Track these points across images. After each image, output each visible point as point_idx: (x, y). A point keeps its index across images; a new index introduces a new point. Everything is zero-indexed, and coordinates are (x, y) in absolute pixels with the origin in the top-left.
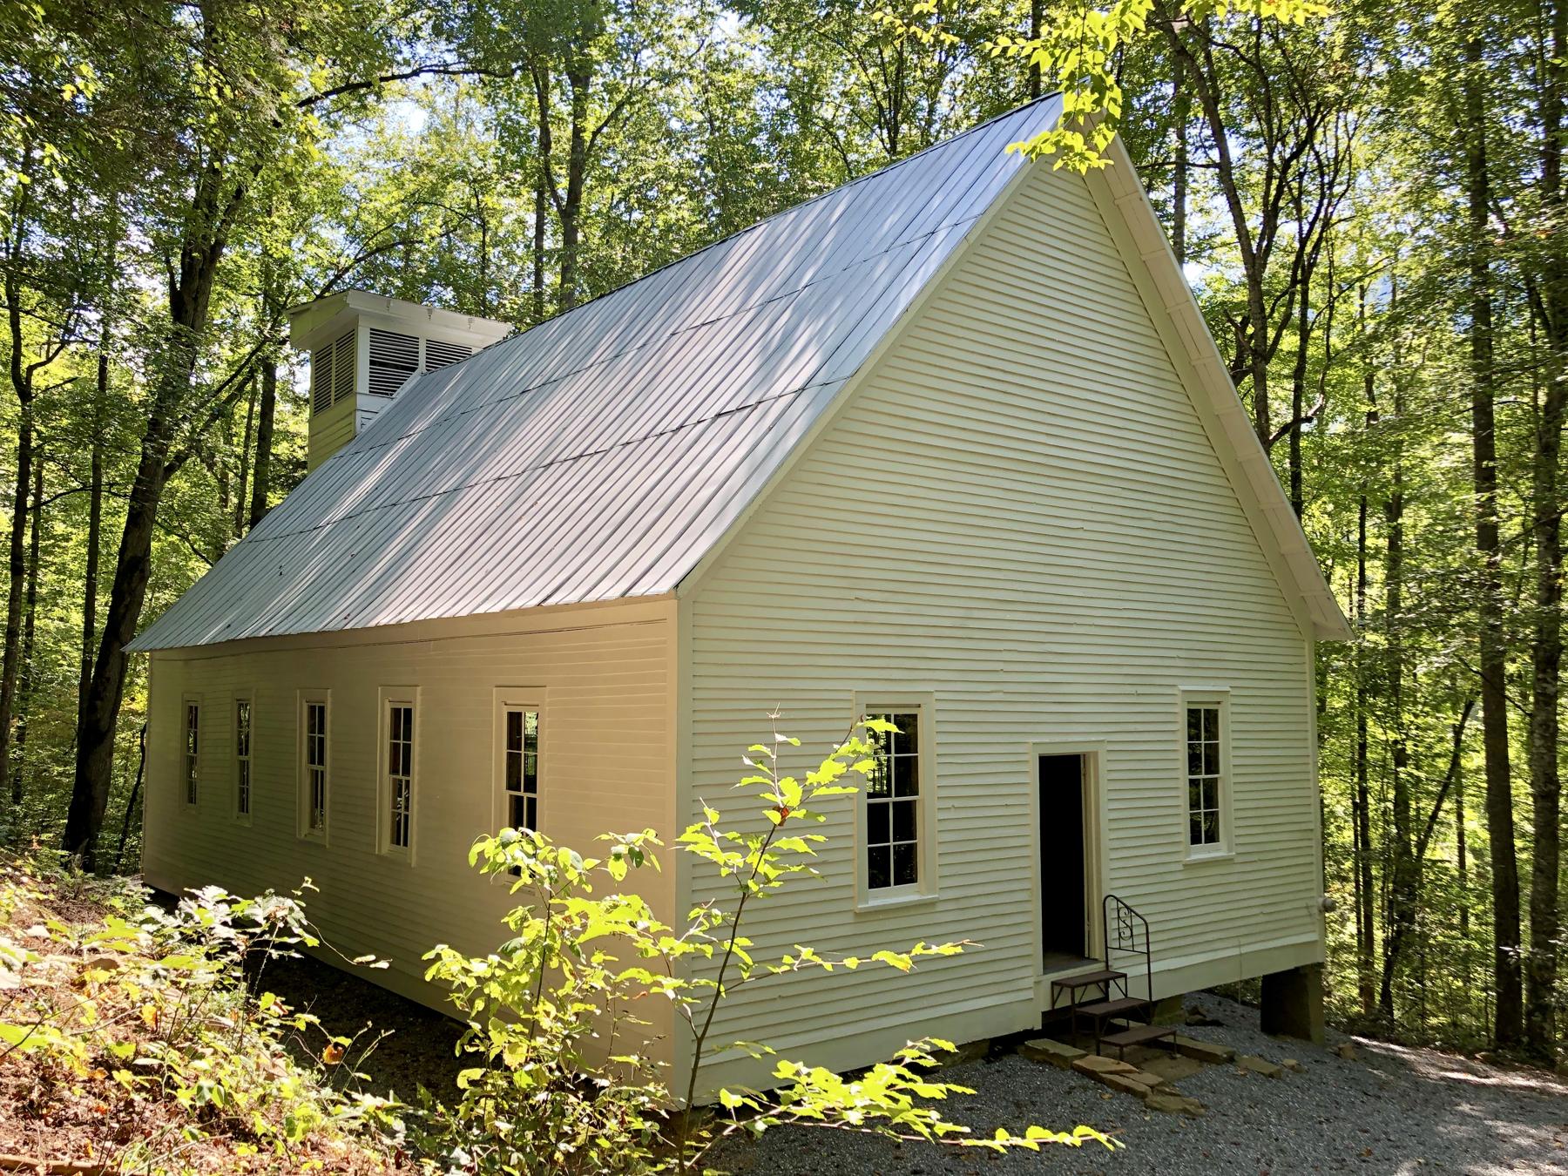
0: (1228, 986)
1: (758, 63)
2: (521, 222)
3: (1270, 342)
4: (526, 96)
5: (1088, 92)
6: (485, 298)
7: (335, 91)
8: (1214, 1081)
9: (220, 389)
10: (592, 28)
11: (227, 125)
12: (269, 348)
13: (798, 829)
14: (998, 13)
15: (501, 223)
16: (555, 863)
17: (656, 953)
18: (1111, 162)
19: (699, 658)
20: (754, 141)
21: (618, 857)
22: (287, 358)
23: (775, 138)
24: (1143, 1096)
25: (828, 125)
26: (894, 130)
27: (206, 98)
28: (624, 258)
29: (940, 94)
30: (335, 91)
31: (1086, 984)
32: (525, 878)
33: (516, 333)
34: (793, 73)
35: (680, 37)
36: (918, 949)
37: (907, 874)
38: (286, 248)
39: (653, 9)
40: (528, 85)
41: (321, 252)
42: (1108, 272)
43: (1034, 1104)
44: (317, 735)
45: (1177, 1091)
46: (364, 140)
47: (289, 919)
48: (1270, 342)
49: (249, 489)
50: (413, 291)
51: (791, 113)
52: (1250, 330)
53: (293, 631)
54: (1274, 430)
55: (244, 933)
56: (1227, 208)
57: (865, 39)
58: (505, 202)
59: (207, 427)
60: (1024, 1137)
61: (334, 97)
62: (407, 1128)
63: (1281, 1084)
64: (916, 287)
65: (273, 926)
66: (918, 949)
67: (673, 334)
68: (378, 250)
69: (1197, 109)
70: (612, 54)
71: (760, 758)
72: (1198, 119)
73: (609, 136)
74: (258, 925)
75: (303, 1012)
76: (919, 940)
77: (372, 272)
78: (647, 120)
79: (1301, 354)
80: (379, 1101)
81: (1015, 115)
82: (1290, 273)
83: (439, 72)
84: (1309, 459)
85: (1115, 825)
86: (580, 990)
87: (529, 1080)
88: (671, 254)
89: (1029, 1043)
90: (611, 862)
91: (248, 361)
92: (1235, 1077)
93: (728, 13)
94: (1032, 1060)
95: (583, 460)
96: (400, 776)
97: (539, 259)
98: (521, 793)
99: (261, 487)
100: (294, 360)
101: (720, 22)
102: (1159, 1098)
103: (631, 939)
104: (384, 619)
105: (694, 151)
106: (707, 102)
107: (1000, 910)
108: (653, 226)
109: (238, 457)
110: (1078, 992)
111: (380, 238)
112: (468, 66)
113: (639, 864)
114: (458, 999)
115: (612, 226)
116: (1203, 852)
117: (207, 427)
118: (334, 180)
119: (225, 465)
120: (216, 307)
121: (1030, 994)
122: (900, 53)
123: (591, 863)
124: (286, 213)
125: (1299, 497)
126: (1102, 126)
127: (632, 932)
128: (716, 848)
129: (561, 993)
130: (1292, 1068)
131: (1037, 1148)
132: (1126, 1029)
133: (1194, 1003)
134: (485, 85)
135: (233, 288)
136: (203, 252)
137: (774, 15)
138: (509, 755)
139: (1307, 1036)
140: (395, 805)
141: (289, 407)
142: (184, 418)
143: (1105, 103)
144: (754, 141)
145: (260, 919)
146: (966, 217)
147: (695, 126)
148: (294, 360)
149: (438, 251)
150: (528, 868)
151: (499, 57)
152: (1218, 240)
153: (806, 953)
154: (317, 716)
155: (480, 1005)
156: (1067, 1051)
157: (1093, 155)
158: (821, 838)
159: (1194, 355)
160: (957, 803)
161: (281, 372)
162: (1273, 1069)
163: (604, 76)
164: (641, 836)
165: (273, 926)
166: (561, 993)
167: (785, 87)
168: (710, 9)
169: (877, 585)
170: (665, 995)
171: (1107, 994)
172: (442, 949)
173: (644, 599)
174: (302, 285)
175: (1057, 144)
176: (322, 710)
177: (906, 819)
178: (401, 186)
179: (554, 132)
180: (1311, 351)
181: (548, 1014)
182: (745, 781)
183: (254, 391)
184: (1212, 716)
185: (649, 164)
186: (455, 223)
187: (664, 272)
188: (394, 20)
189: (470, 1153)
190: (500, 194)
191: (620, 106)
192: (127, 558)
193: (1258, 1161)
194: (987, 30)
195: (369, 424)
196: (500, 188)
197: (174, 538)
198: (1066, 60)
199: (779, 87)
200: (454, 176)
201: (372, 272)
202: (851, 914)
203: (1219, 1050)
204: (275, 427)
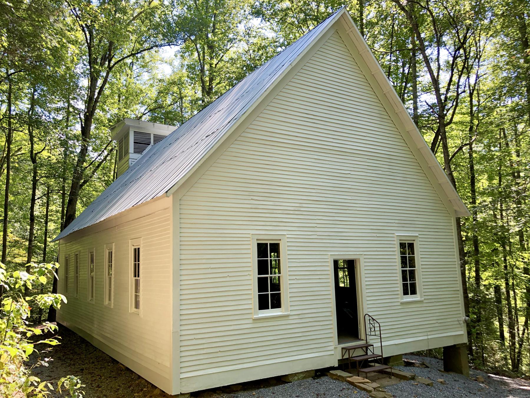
0: (418, 352)
8: (403, 387)
24: (370, 391)
31: (355, 349)
37: (277, 304)
63: (433, 388)
85: (368, 287)
92: (413, 385)
94: (332, 378)
110: (351, 351)
116: (410, 298)
121: (332, 352)
130: (441, 382)
139: (461, 373)
159: (396, 109)
160: (298, 277)
162: (430, 382)
184: (411, 246)
192: (68, 215)
195: (134, 163)
202: (251, 320)
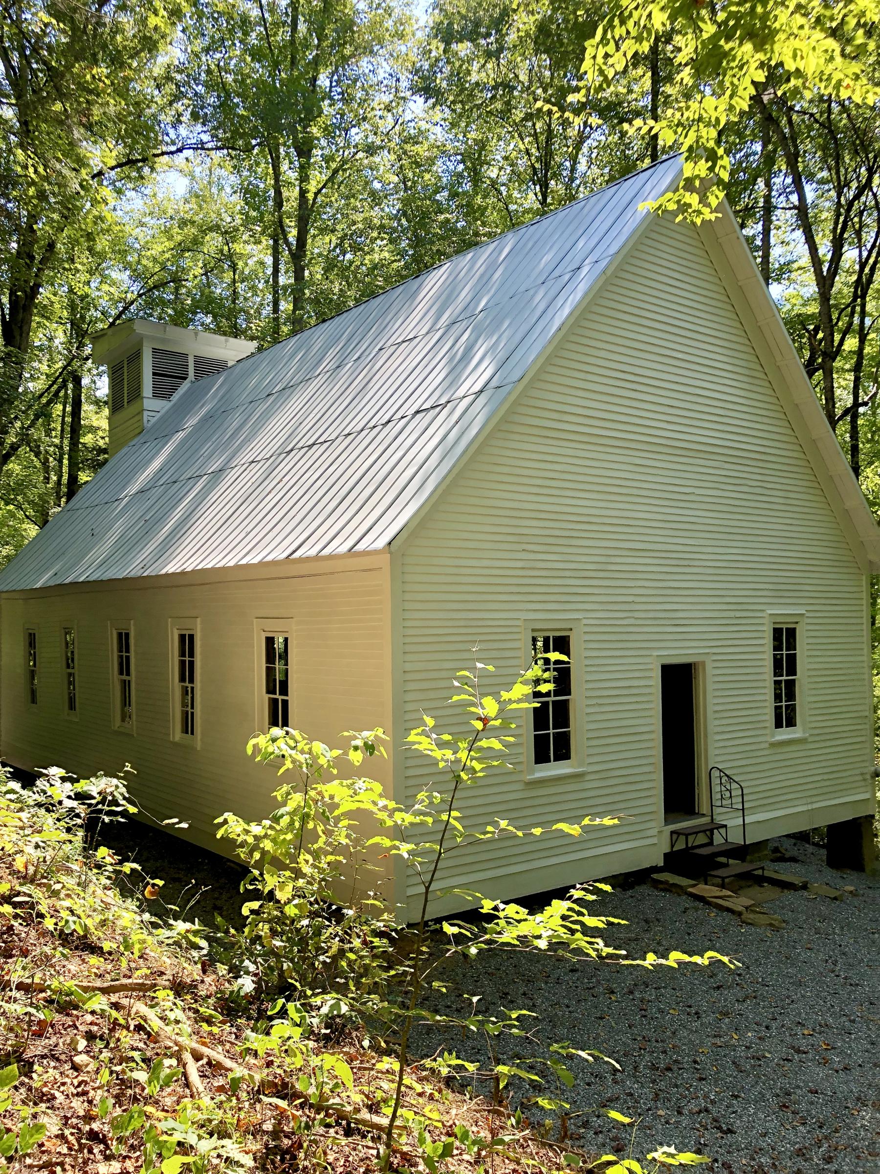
0: (801, 832)
1: (439, 136)
2: (262, 263)
3: (836, 344)
4: (263, 165)
5: (703, 161)
6: (236, 323)
7: (120, 165)
9: (41, 396)
10: (312, 111)
11: (42, 196)
12: (76, 364)
13: (495, 733)
14: (625, 91)
15: (246, 264)
16: (310, 752)
17: (392, 824)
18: (720, 215)
19: (407, 597)
20: (438, 197)
21: (356, 748)
22: (89, 370)
23: (454, 195)
24: (740, 914)
25: (494, 183)
26: (545, 186)
27: (26, 176)
28: (341, 290)
29: (580, 156)
30: (120, 165)
31: (697, 833)
32: (288, 764)
33: (260, 349)
34: (466, 143)
35: (381, 118)
36: (586, 821)
37: (563, 752)
38: (86, 287)
39: (359, 95)
40: (265, 157)
41: (112, 290)
42: (742, 393)
43: (658, 920)
44: (124, 654)
45: (764, 910)
46: (141, 202)
47: (115, 793)
48: (836, 344)
49: (65, 469)
50: (181, 319)
51: (466, 174)
52: (820, 335)
53: (105, 577)
54: (839, 412)
55: (83, 804)
56: (803, 239)
57: (522, 115)
58: (249, 248)
59: (33, 424)
60: (667, 959)
61: (119, 169)
62: (210, 945)
64: (566, 311)
65: (105, 798)
66: (586, 821)
67: (381, 349)
68: (156, 287)
69: (782, 165)
70: (329, 132)
71: (465, 681)
72: (780, 171)
73: (326, 195)
74: (94, 798)
75: (128, 861)
76: (587, 815)
77: (151, 304)
78: (355, 182)
79: (860, 352)
80: (188, 925)
81: (641, 175)
82: (852, 290)
83: (197, 149)
84: (864, 433)
86: (330, 844)
87: (297, 911)
88: (377, 286)
89: (655, 876)
90: (351, 752)
91: (61, 373)
92: (808, 900)
93: (416, 98)
94: (656, 888)
95: (315, 447)
96: (187, 684)
97: (276, 292)
98: (277, 696)
99: (74, 468)
100: (95, 372)
101: (411, 104)
102: (752, 916)
103: (372, 813)
104: (171, 568)
105: (392, 206)
106: (401, 167)
107: (632, 779)
108: (362, 264)
109: (56, 446)
110: (691, 839)
111: (156, 277)
112: (219, 144)
113: (371, 754)
114: (242, 853)
115: (330, 265)
116: (785, 734)
117: (33, 424)
118: (121, 234)
119: (47, 452)
120: (35, 332)
121: (654, 840)
122: (549, 126)
123: (336, 753)
124: (85, 261)
125: (857, 463)
126: (715, 188)
127: (374, 809)
128: (434, 747)
129: (315, 846)
130: (851, 892)
131: (676, 966)
132: (726, 865)
133: (776, 845)
134: (232, 158)
135: (48, 318)
136: (24, 292)
137: (451, 98)
138: (267, 668)
140: (184, 705)
141: (92, 408)
142: (16, 418)
143: (717, 170)
144: (438, 197)
145: (95, 794)
146: (604, 255)
147: (392, 185)
148: (95, 372)
149: (200, 287)
150: (290, 756)
151: (242, 136)
152: (795, 266)
153: (503, 824)
154: (124, 640)
155: (257, 856)
156: (683, 881)
157: (706, 210)
158: (511, 739)
161: (85, 381)
162: (837, 893)
163: (322, 149)
164: (373, 733)
165: (105, 798)
166: (315, 846)
167: (461, 154)
168: (402, 95)
169: (536, 540)
170: (401, 856)
171: (711, 839)
172: (229, 816)
173: (365, 553)
174: (99, 315)
175: (678, 202)
176: (127, 635)
177: (562, 713)
178: (170, 238)
179: (285, 193)
180: (867, 350)
181: (307, 862)
182: (455, 698)
183: (66, 395)
184: (792, 633)
185: (359, 217)
186: (212, 265)
187: (373, 301)
188: (162, 109)
189: (255, 963)
190: (245, 242)
191: (335, 172)
193: (827, 961)
194: (616, 105)
195: (153, 420)
196: (245, 237)
197: (11, 507)
198: (686, 136)
199: (457, 154)
200: (211, 229)
201: (151, 304)
203: (797, 881)
204: (82, 422)
